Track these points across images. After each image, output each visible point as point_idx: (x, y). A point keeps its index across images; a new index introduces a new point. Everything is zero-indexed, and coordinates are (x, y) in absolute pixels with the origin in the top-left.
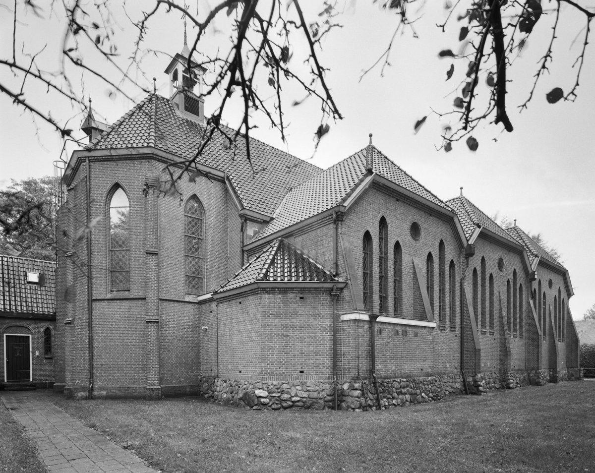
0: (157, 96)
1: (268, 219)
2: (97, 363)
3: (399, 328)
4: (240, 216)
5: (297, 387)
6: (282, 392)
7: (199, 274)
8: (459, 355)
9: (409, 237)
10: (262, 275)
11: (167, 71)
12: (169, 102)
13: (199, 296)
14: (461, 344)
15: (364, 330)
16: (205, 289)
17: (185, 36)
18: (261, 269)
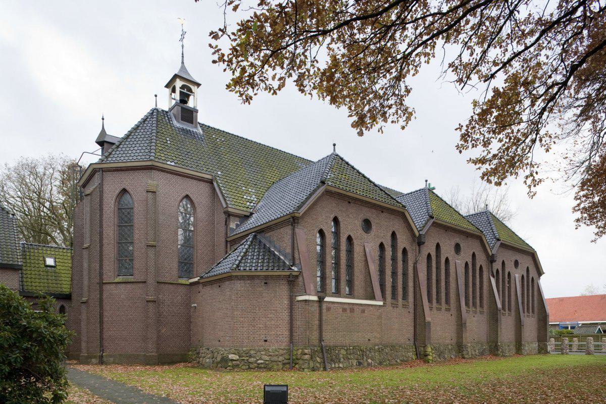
0: (157, 110)
1: (248, 214)
2: (106, 335)
3: (346, 306)
4: (225, 213)
5: (262, 353)
6: (250, 356)
7: (190, 260)
8: (413, 328)
9: (361, 231)
10: (235, 266)
11: (167, 86)
12: (168, 114)
13: (191, 278)
14: (414, 319)
15: (315, 308)
16: (195, 272)
17: (183, 57)
18: (238, 257)
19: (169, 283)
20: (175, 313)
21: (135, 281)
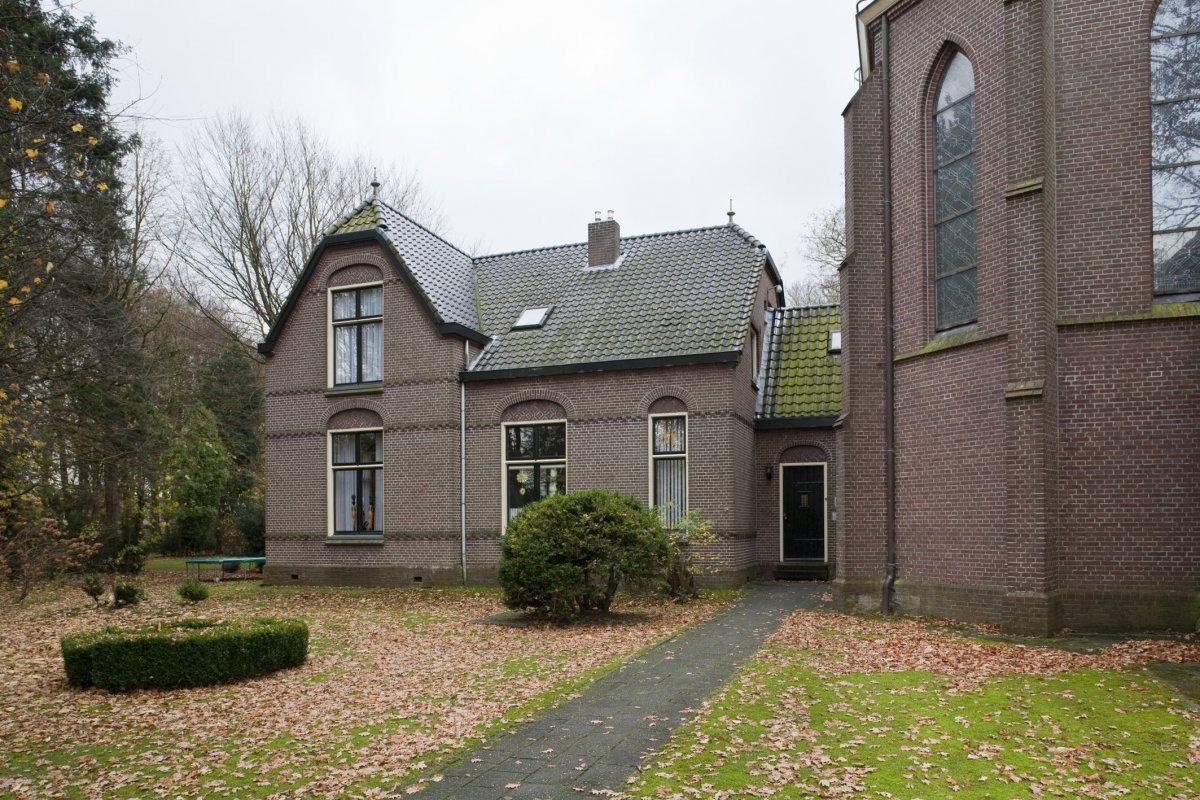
2: (903, 523)
19: (1108, 325)
20: (1138, 437)
21: (981, 338)
